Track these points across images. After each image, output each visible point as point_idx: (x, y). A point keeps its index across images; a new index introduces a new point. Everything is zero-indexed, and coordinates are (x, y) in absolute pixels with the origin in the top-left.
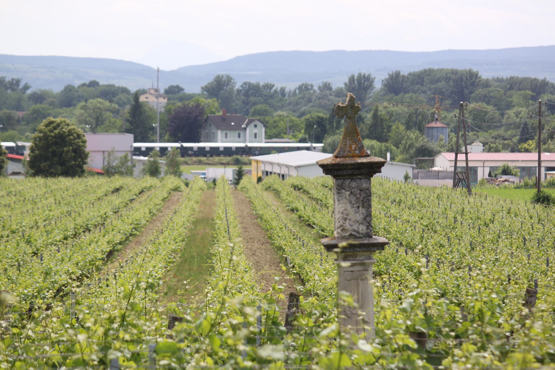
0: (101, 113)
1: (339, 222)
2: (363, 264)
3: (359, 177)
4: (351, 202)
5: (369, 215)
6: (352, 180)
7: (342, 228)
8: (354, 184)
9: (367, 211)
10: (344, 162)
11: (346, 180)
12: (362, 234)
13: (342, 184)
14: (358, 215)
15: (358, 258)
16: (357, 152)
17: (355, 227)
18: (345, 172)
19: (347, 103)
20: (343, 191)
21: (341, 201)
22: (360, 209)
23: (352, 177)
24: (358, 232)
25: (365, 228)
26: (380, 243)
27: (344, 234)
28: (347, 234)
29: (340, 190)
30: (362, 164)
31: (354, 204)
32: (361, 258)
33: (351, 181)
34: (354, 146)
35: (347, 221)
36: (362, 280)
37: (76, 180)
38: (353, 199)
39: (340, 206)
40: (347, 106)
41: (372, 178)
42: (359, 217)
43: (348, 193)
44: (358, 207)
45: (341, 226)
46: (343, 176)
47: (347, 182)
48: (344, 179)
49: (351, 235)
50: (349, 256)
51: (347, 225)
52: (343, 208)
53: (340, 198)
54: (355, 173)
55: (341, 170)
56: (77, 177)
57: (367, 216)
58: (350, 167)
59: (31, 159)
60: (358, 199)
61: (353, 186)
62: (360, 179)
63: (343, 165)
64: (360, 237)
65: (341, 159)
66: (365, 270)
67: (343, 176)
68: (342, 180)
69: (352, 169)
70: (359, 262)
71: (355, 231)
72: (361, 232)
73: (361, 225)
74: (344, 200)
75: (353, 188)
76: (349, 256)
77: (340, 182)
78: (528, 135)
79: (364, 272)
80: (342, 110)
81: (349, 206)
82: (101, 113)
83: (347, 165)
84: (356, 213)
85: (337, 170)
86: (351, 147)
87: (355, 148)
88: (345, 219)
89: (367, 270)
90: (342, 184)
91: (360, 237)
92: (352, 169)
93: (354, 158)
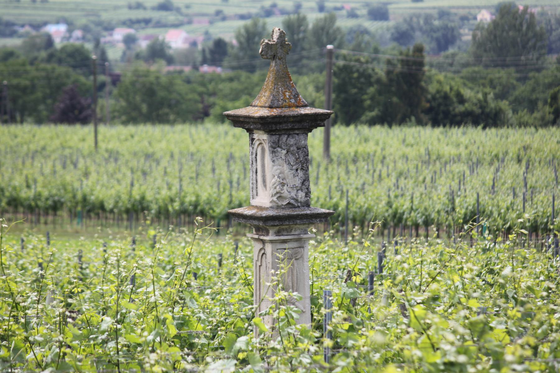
1: (275, 188)
2: (299, 240)
3: (297, 132)
5: (305, 181)
6: (289, 135)
7: (278, 195)
8: (292, 141)
9: (304, 174)
11: (283, 136)
12: (301, 202)
13: (279, 141)
15: (293, 233)
18: (284, 126)
19: (275, 40)
20: (279, 149)
21: (277, 162)
22: (299, 171)
23: (289, 132)
24: (297, 200)
25: (304, 194)
26: (318, 214)
28: (285, 203)
29: (275, 148)
30: (306, 115)
31: (292, 166)
32: (297, 233)
33: (288, 137)
34: (287, 93)
35: (285, 187)
36: (296, 259)
37: (492, 132)
38: (292, 159)
39: (275, 168)
40: (276, 44)
41: (310, 134)
43: (284, 152)
44: (297, 170)
45: (277, 193)
46: (280, 130)
47: (284, 138)
48: (280, 135)
49: (289, 203)
50: (283, 230)
51: (285, 193)
52: (278, 171)
53: (275, 158)
54: (296, 127)
55: (280, 123)
56: (506, 127)
57: (304, 181)
58: (292, 120)
60: (297, 159)
61: (292, 143)
62: (298, 134)
63: (285, 116)
64: (299, 207)
66: (300, 247)
67: (280, 130)
68: (278, 136)
69: (293, 122)
70: (296, 237)
71: (294, 199)
72: (299, 200)
73: (300, 191)
74: (280, 160)
75: (291, 146)
76: (283, 230)
77: (275, 138)
78: (558, 85)
79: (299, 250)
80: (271, 48)
81: (286, 168)
83: (289, 117)
84: (294, 176)
85: (276, 124)
86: (285, 96)
87: (289, 96)
88: (283, 185)
89: (303, 247)
90: (279, 141)
91: (299, 207)
92: (293, 122)
93: (291, 109)
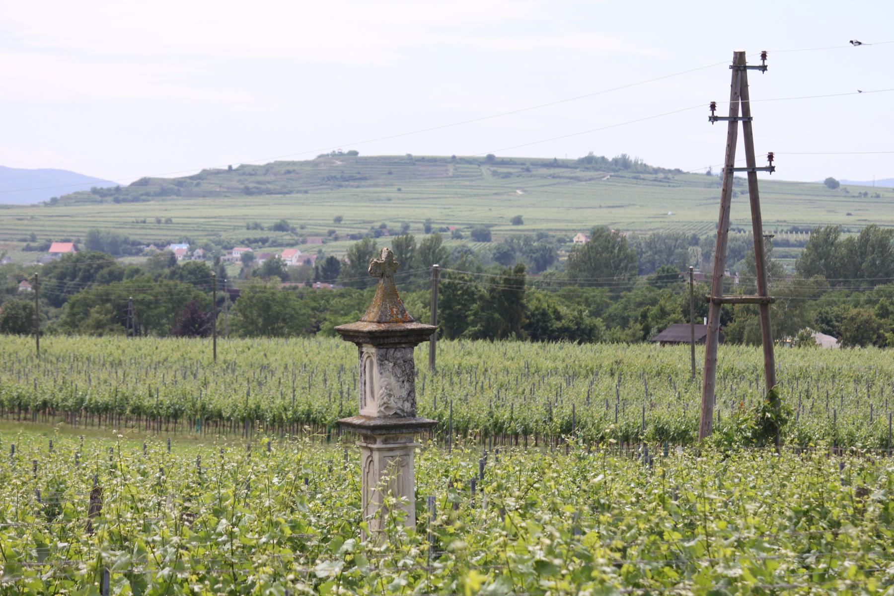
0: (44, 295)
3: (403, 346)
4: (396, 376)
5: (411, 392)
8: (399, 354)
10: (390, 329)
14: (403, 390)
15: (399, 441)
16: (400, 316)
17: (399, 405)
18: (391, 341)
20: (387, 362)
21: (384, 374)
23: (396, 346)
24: (403, 411)
27: (387, 413)
30: (413, 330)
35: (392, 398)
38: (399, 372)
40: (385, 263)
42: (404, 393)
43: (391, 364)
46: (387, 344)
47: (392, 351)
48: (387, 349)
49: (396, 413)
50: (390, 438)
51: (392, 403)
55: (388, 338)
59: (590, 247)
63: (392, 331)
65: (387, 325)
67: (387, 344)
69: (399, 336)
70: (402, 445)
71: (400, 409)
75: (398, 359)
76: (390, 438)
77: (383, 351)
81: (393, 380)
82: (44, 295)
83: (396, 332)
85: (384, 338)
88: (390, 395)
92: (399, 336)
